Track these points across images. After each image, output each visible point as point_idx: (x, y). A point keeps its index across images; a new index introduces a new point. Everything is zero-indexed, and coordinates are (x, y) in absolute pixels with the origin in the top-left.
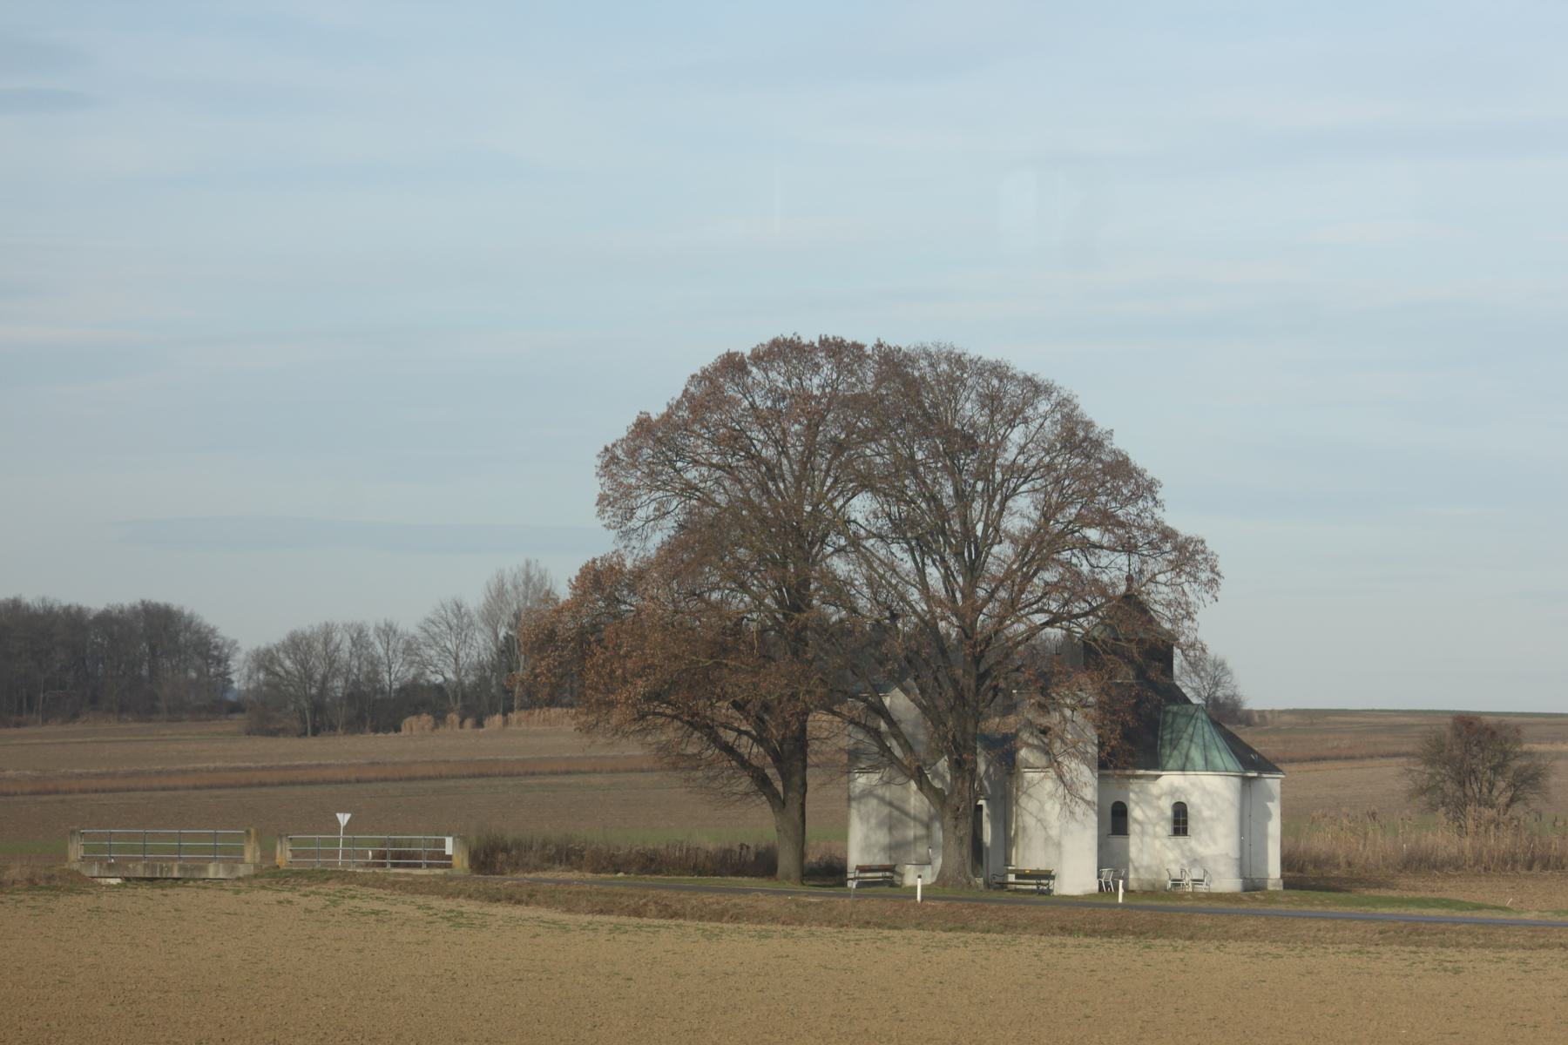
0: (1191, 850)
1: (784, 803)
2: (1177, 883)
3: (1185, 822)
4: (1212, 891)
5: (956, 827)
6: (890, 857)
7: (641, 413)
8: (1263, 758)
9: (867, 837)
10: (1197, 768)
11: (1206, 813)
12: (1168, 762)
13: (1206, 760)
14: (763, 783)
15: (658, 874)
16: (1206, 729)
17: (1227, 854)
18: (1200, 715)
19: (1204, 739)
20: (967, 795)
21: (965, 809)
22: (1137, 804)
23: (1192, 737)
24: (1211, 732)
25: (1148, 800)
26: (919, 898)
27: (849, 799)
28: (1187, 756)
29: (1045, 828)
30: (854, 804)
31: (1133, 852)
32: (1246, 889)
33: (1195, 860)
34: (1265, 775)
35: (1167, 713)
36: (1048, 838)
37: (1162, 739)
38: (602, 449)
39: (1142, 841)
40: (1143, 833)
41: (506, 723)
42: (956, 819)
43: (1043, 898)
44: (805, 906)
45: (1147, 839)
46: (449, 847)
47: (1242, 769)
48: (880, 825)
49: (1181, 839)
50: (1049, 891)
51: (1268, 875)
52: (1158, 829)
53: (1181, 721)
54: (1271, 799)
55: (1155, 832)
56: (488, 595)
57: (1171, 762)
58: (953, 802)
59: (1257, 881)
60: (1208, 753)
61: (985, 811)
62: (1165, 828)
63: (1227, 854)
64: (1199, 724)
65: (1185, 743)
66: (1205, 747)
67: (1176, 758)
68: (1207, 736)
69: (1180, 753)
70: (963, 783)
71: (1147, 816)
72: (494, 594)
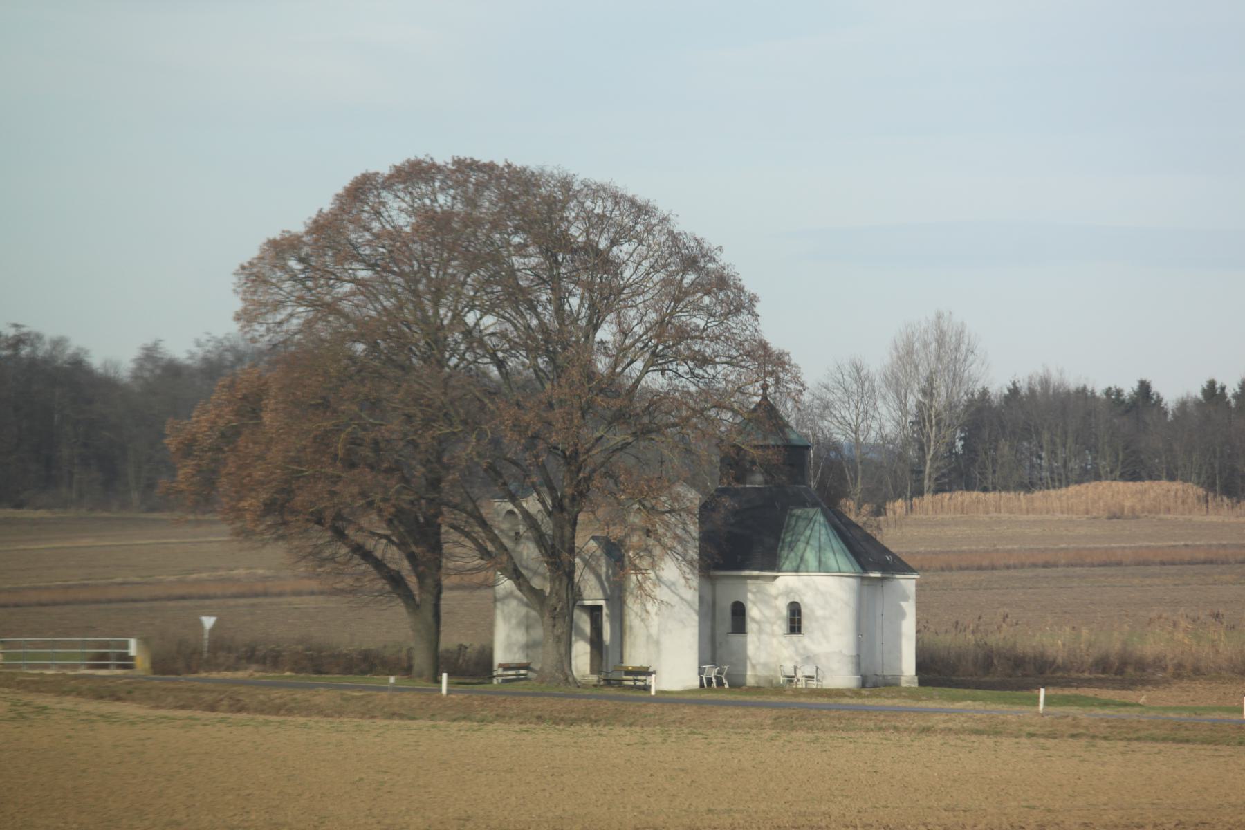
0: (805, 648)
1: (418, 606)
2: (790, 679)
3: (800, 621)
4: (825, 687)
5: (554, 626)
6: (527, 656)
7: (284, 232)
8: (899, 559)
9: (508, 636)
10: (810, 569)
11: (819, 612)
12: (784, 563)
13: (820, 561)
14: (396, 581)
15: (966, 700)
16: (823, 531)
17: (841, 652)
18: (818, 518)
19: (820, 541)
20: (565, 596)
21: (562, 608)
22: (754, 603)
23: (809, 538)
24: (828, 535)
25: (766, 600)
26: (444, 691)
27: (495, 600)
28: (802, 558)
29: (647, 627)
30: (499, 604)
31: (751, 650)
32: (863, 685)
33: (808, 658)
34: (897, 576)
35: (792, 516)
36: (649, 637)
37: (783, 542)
38: (237, 267)
39: (759, 639)
40: (760, 631)
41: (911, 509)
42: (554, 618)
43: (641, 694)
44: (347, 700)
45: (764, 637)
46: (133, 648)
47: (861, 571)
48: (519, 624)
49: (795, 637)
50: (647, 688)
51: (902, 672)
52: (776, 628)
53: (802, 524)
54: (906, 599)
55: (773, 631)
56: (895, 354)
57: (787, 563)
58: (551, 603)
59: (889, 678)
60: (822, 556)
61: (605, 611)
62: (781, 627)
63: (841, 652)
64: (817, 527)
65: (801, 546)
66: (820, 549)
67: (790, 560)
68: (823, 539)
69: (796, 555)
70: (560, 584)
71: (764, 616)
72: (902, 353)
